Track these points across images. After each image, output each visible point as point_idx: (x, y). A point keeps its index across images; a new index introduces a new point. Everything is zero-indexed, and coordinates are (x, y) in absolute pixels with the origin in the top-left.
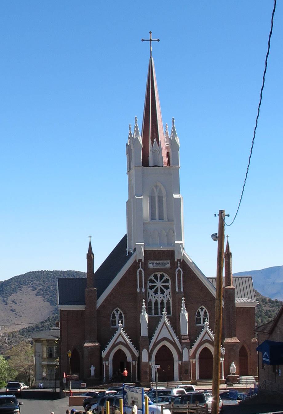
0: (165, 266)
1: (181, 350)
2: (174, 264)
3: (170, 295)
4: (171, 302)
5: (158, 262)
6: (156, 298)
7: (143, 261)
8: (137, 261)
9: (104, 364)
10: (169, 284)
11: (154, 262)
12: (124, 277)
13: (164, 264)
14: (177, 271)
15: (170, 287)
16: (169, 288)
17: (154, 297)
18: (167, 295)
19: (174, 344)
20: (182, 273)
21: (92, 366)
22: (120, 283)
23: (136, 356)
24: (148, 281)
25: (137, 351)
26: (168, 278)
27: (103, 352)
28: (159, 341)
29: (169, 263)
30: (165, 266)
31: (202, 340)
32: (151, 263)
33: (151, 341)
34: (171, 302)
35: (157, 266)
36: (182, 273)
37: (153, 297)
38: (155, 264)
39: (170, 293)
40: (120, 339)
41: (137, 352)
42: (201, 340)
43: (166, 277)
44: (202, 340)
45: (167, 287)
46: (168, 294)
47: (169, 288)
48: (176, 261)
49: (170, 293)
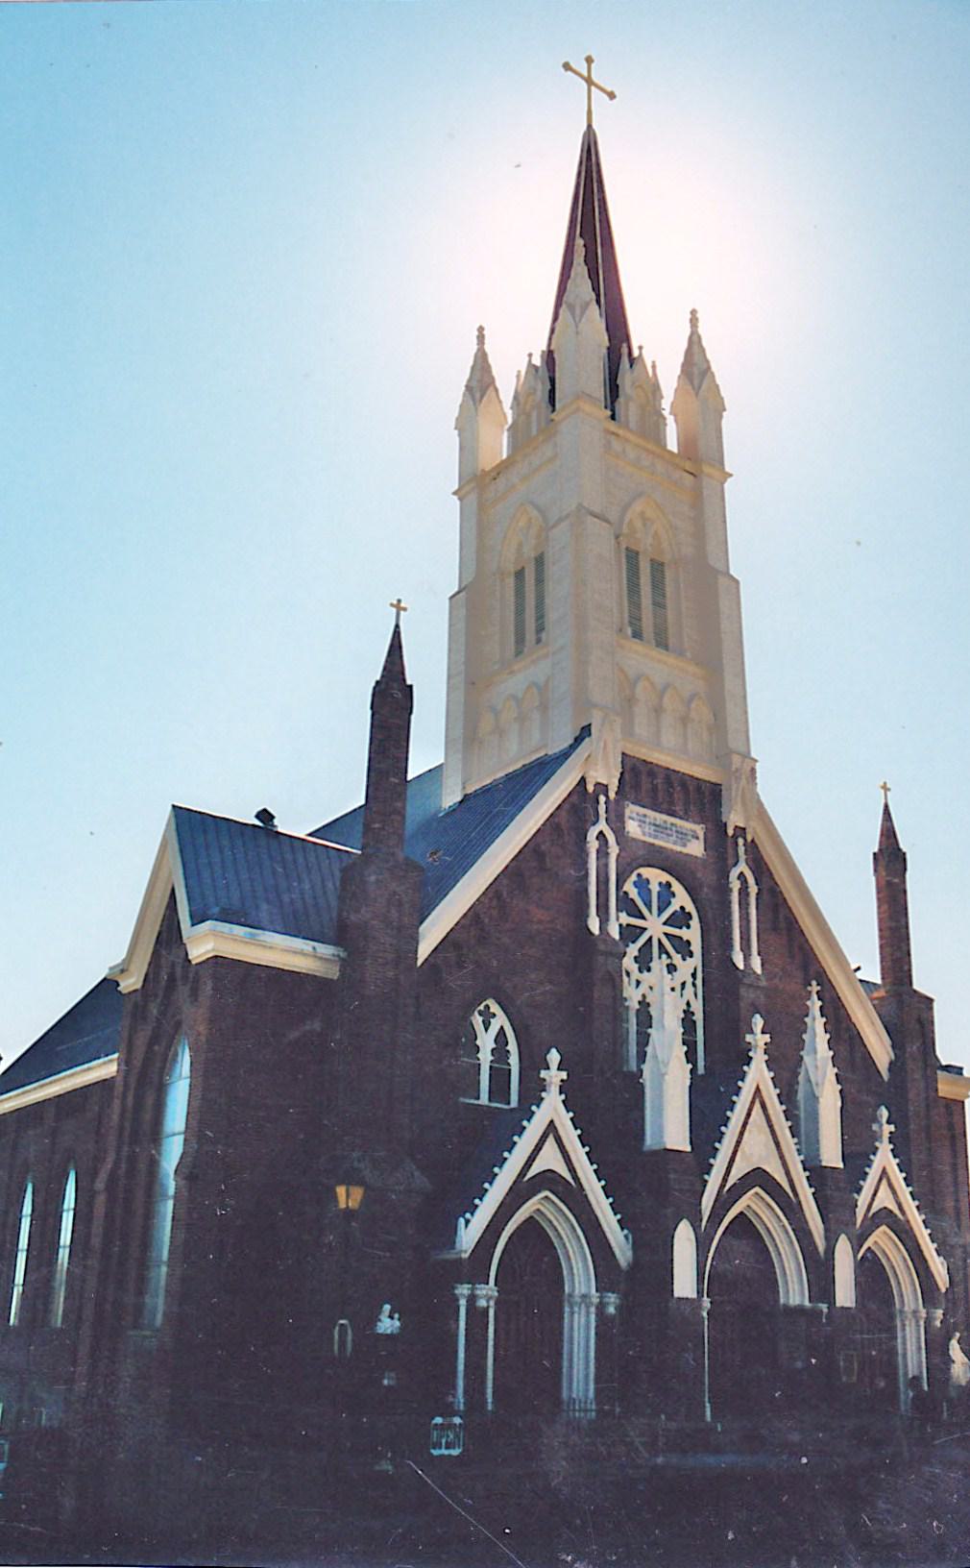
0: (685, 845)
1: (821, 1244)
2: (721, 841)
3: (694, 985)
4: (699, 1017)
5: (661, 818)
6: (643, 988)
7: (612, 795)
8: (590, 788)
9: (463, 1302)
10: (693, 934)
11: (645, 816)
12: (532, 850)
13: (683, 837)
14: (734, 873)
15: (696, 947)
16: (691, 955)
17: (638, 983)
18: (683, 984)
19: (791, 1209)
20: (753, 889)
21: (387, 1307)
22: (513, 872)
23: (618, 1265)
24: (476, 1013)
25: (626, 1237)
26: (690, 908)
27: (467, 1222)
28: (573, 1178)
29: (701, 836)
30: (685, 845)
31: (531, 1174)
32: (634, 815)
33: (706, 1181)
34: (699, 1017)
35: (656, 837)
36: (753, 889)
37: (634, 983)
38: (650, 823)
39: (694, 975)
40: (549, 1159)
41: (623, 1238)
42: (722, 1186)
43: (682, 899)
44: (531, 1174)
45: (684, 948)
46: (690, 980)
47: (691, 955)
48: (730, 832)
49: (694, 975)
